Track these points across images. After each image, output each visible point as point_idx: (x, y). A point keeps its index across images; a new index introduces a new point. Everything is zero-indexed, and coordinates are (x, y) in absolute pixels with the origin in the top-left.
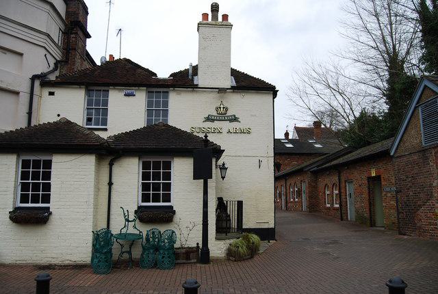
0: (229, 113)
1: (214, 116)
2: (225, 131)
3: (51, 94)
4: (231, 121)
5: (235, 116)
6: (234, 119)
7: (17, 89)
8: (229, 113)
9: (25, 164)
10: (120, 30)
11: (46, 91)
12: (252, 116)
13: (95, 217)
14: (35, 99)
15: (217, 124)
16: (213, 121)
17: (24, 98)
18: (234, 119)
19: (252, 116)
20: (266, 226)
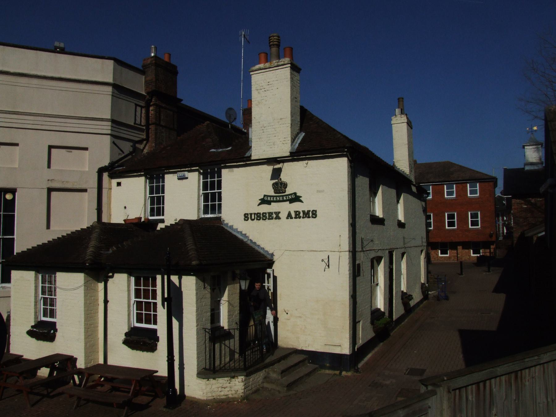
0: (289, 191)
1: (270, 196)
2: (283, 215)
3: (119, 184)
4: (291, 201)
5: (295, 194)
6: (296, 198)
7: (83, 187)
8: (289, 191)
9: (185, 176)
10: (340, 236)
11: (114, 182)
12: (319, 191)
13: (123, 388)
14: (105, 192)
15: (274, 207)
16: (269, 203)
17: (92, 195)
18: (296, 198)
19: (319, 191)
20: (337, 351)
